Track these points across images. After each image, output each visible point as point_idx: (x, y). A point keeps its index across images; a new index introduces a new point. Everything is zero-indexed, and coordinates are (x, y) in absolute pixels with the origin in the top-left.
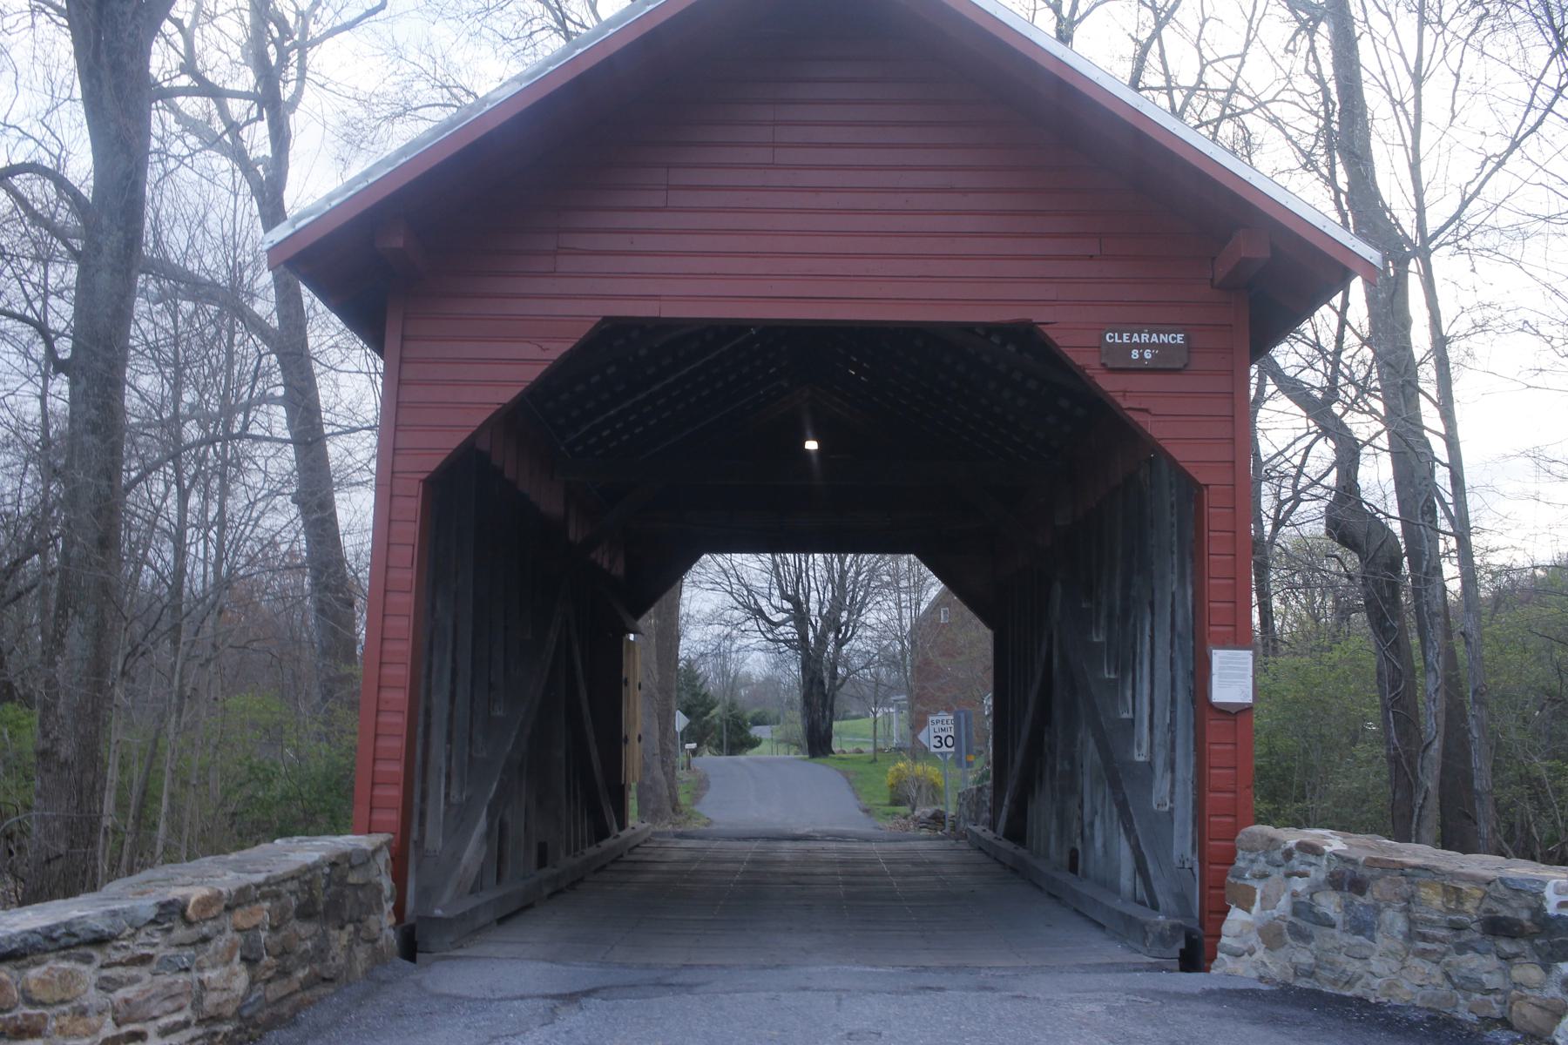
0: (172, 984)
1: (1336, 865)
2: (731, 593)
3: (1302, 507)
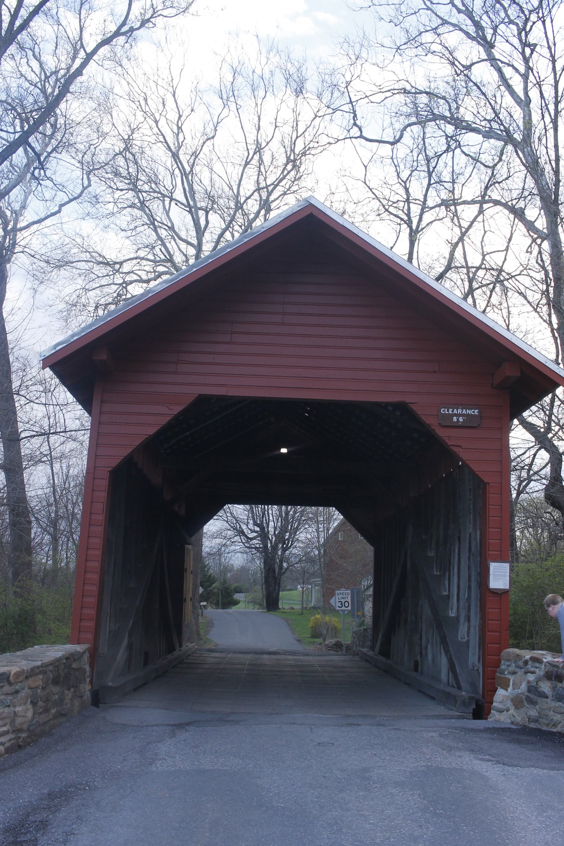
0: (2, 712)
1: (549, 668)
2: (227, 522)
3: (532, 484)
